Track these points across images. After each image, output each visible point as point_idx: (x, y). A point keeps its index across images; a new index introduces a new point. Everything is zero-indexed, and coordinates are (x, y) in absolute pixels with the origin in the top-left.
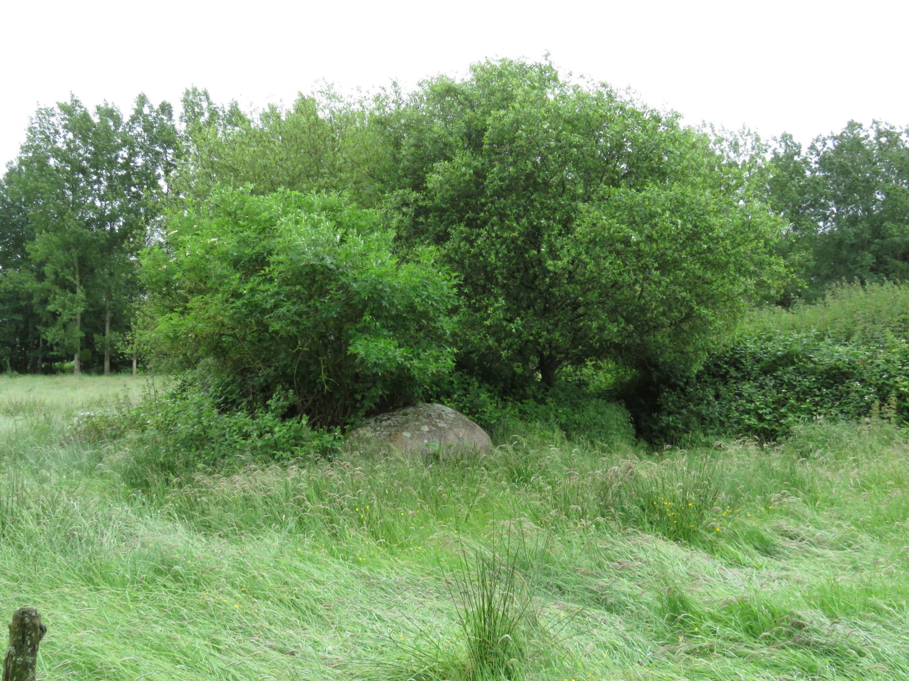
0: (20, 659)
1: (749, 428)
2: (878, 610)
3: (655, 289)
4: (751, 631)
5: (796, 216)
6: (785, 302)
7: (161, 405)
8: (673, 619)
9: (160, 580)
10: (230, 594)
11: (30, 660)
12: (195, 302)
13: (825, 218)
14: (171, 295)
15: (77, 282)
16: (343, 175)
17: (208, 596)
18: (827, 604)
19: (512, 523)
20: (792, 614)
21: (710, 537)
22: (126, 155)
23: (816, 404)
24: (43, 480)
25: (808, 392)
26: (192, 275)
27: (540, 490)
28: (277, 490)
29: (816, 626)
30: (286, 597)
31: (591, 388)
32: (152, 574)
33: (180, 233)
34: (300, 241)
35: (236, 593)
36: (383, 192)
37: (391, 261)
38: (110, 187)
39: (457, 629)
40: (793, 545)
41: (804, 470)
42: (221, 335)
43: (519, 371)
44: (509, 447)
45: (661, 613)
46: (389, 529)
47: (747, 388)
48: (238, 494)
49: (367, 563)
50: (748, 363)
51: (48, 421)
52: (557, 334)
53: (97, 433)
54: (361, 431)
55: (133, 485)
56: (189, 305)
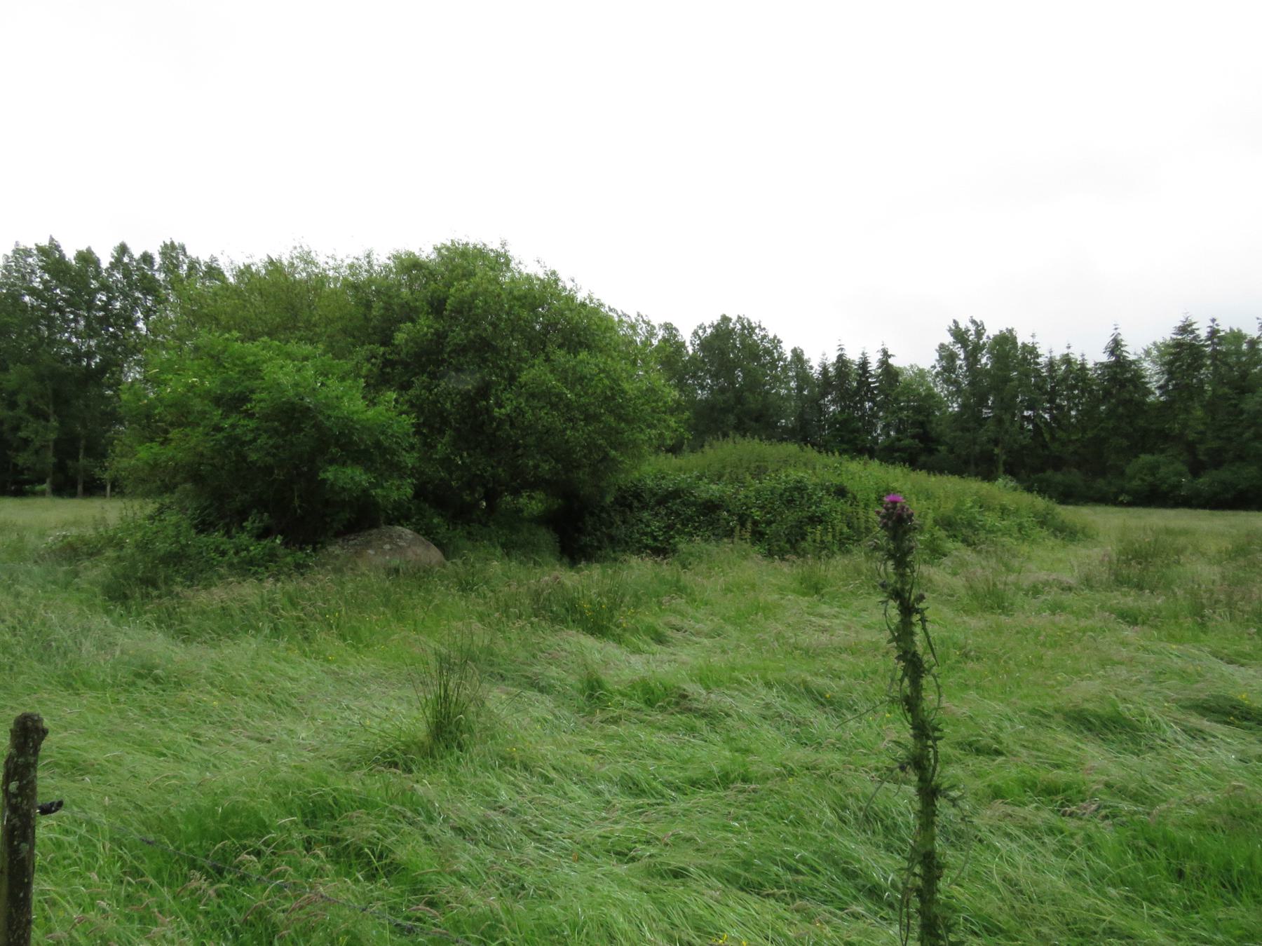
0: (21, 760)
1: (647, 547)
2: (739, 682)
3: (577, 435)
4: (650, 703)
5: (681, 385)
6: (675, 450)
7: (139, 527)
8: (591, 696)
9: (140, 683)
10: (210, 693)
11: (32, 760)
12: (174, 434)
13: (703, 388)
14: (151, 425)
15: (51, 411)
16: (318, 330)
17: (188, 695)
18: (706, 679)
19: (456, 622)
20: (679, 688)
21: (619, 631)
22: (104, 298)
23: (696, 528)
24: (18, 595)
25: (690, 519)
26: (173, 410)
27: (485, 597)
28: (254, 600)
29: (696, 696)
30: (263, 694)
31: (525, 514)
32: (131, 678)
33: (161, 372)
34: (284, 380)
35: (215, 691)
36: (354, 346)
37: (361, 404)
38: (88, 325)
39: (415, 713)
40: (679, 635)
41: (687, 578)
42: (200, 464)
43: (468, 499)
44: (459, 562)
45: (582, 692)
46: (356, 633)
47: (646, 515)
48: (216, 604)
49: (335, 662)
50: (646, 496)
51: (21, 538)
52: (500, 470)
53: (73, 552)
54: (330, 549)
55: (111, 598)
56: (170, 436)
